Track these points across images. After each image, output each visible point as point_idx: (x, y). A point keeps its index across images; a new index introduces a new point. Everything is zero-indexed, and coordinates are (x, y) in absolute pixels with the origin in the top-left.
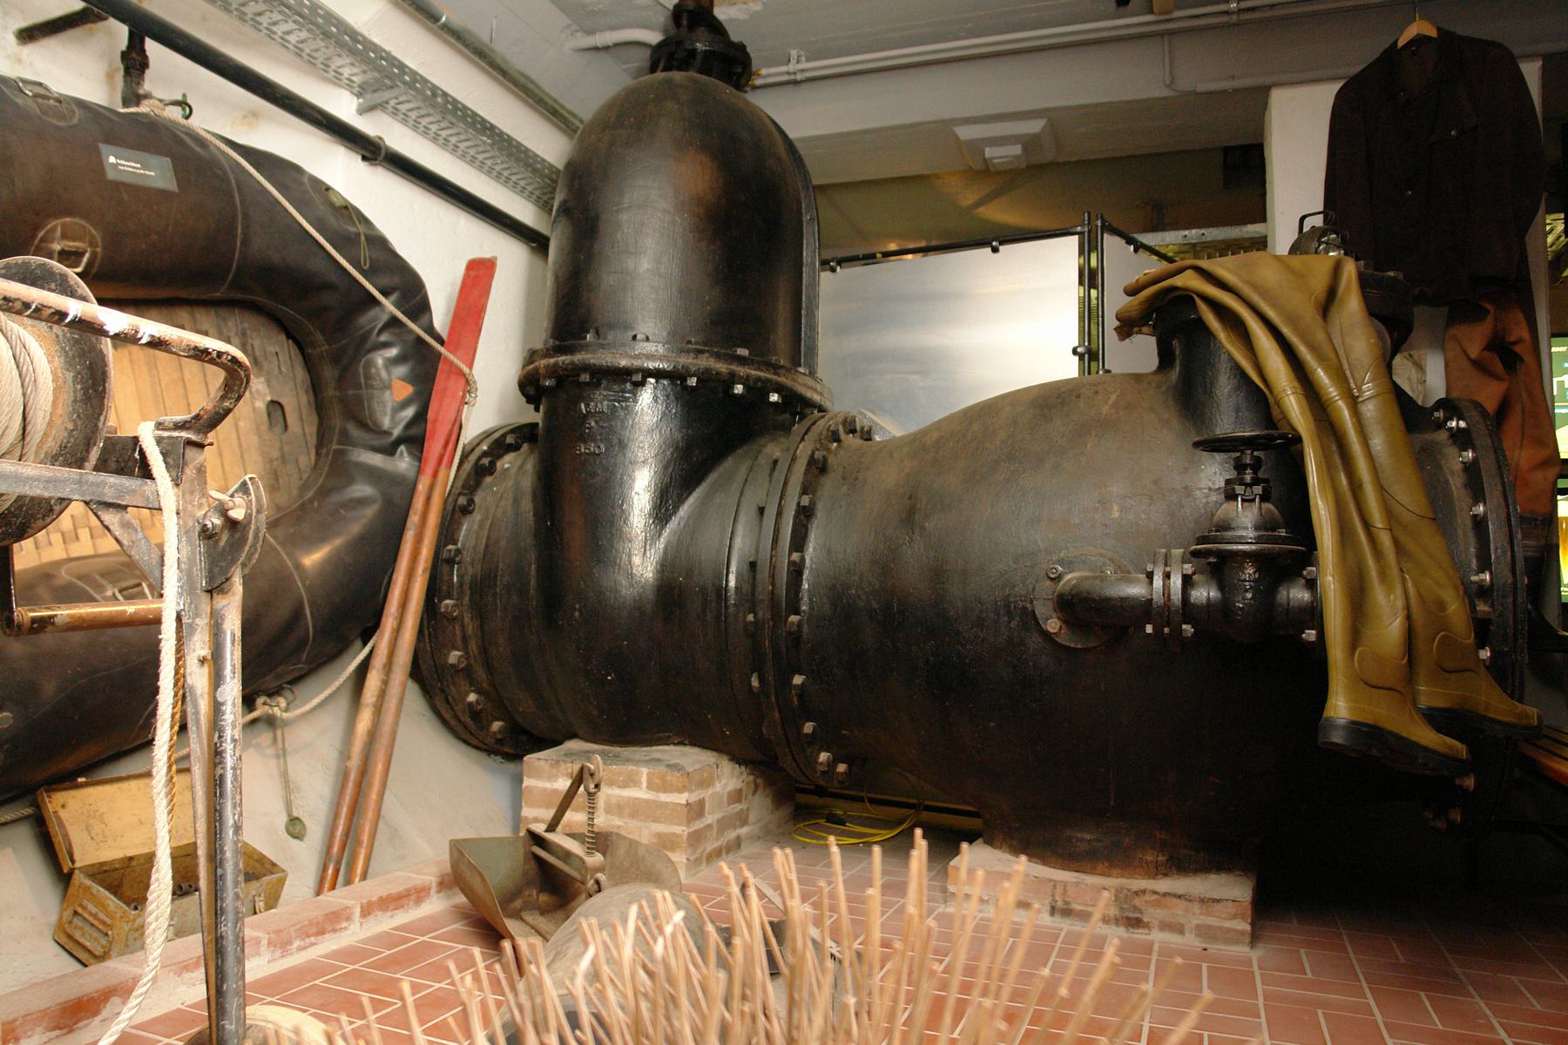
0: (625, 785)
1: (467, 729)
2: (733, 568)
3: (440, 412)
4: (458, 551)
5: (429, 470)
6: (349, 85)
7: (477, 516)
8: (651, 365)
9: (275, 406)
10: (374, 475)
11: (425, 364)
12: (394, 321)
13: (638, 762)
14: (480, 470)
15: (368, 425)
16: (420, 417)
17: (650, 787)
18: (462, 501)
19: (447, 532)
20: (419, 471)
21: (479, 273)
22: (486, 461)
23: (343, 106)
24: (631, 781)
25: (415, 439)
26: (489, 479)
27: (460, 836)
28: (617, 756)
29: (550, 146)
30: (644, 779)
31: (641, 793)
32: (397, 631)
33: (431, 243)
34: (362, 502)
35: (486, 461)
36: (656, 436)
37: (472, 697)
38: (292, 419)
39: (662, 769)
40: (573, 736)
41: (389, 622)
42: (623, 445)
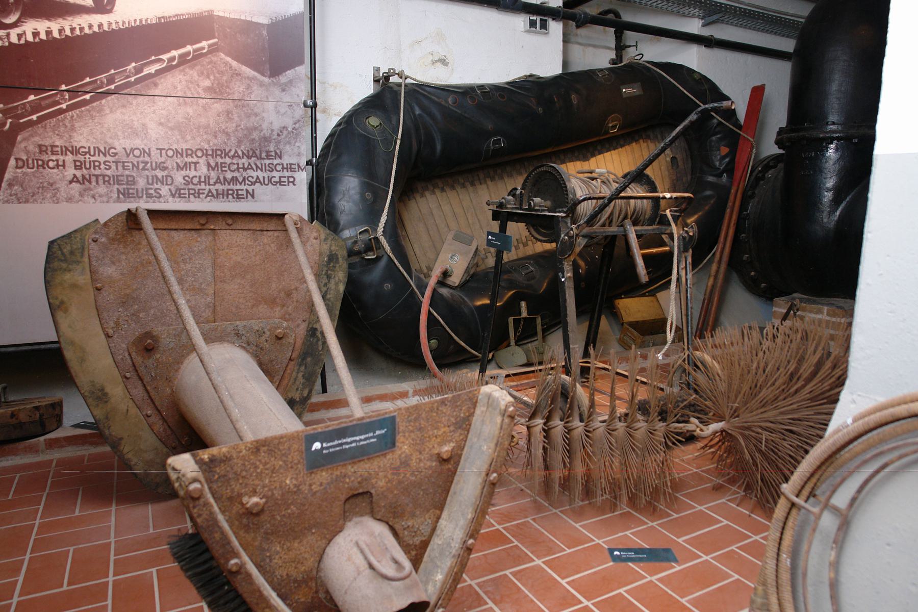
0: (817, 313)
1: (753, 287)
2: (674, 134)
3: (741, 158)
4: (748, 214)
5: (736, 184)
6: (699, 17)
7: (756, 199)
8: (835, 135)
9: (673, 159)
10: (712, 186)
11: (733, 139)
12: (720, 123)
13: (823, 304)
14: (757, 179)
15: (711, 165)
16: (732, 161)
17: (828, 314)
18: (750, 193)
19: (743, 207)
20: (732, 184)
21: (758, 93)
22: (760, 175)
23: (694, 26)
24: (820, 312)
25: (730, 170)
26: (762, 182)
27: (766, 90)
28: (814, 301)
29: (788, 45)
30: (825, 311)
31: (824, 317)
32: (724, 244)
33: (731, 78)
34: (709, 197)
35: (760, 175)
36: (837, 166)
37: (753, 274)
38: (680, 163)
39: (834, 308)
40: (796, 292)
41: (722, 239)
42: (821, 171)
